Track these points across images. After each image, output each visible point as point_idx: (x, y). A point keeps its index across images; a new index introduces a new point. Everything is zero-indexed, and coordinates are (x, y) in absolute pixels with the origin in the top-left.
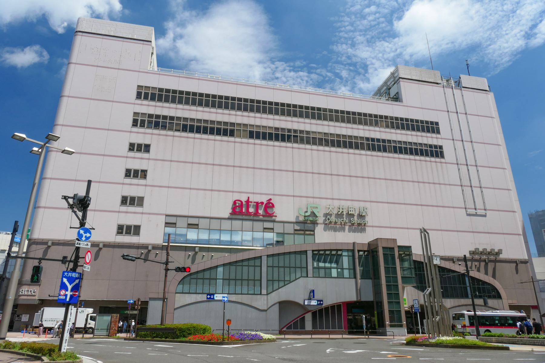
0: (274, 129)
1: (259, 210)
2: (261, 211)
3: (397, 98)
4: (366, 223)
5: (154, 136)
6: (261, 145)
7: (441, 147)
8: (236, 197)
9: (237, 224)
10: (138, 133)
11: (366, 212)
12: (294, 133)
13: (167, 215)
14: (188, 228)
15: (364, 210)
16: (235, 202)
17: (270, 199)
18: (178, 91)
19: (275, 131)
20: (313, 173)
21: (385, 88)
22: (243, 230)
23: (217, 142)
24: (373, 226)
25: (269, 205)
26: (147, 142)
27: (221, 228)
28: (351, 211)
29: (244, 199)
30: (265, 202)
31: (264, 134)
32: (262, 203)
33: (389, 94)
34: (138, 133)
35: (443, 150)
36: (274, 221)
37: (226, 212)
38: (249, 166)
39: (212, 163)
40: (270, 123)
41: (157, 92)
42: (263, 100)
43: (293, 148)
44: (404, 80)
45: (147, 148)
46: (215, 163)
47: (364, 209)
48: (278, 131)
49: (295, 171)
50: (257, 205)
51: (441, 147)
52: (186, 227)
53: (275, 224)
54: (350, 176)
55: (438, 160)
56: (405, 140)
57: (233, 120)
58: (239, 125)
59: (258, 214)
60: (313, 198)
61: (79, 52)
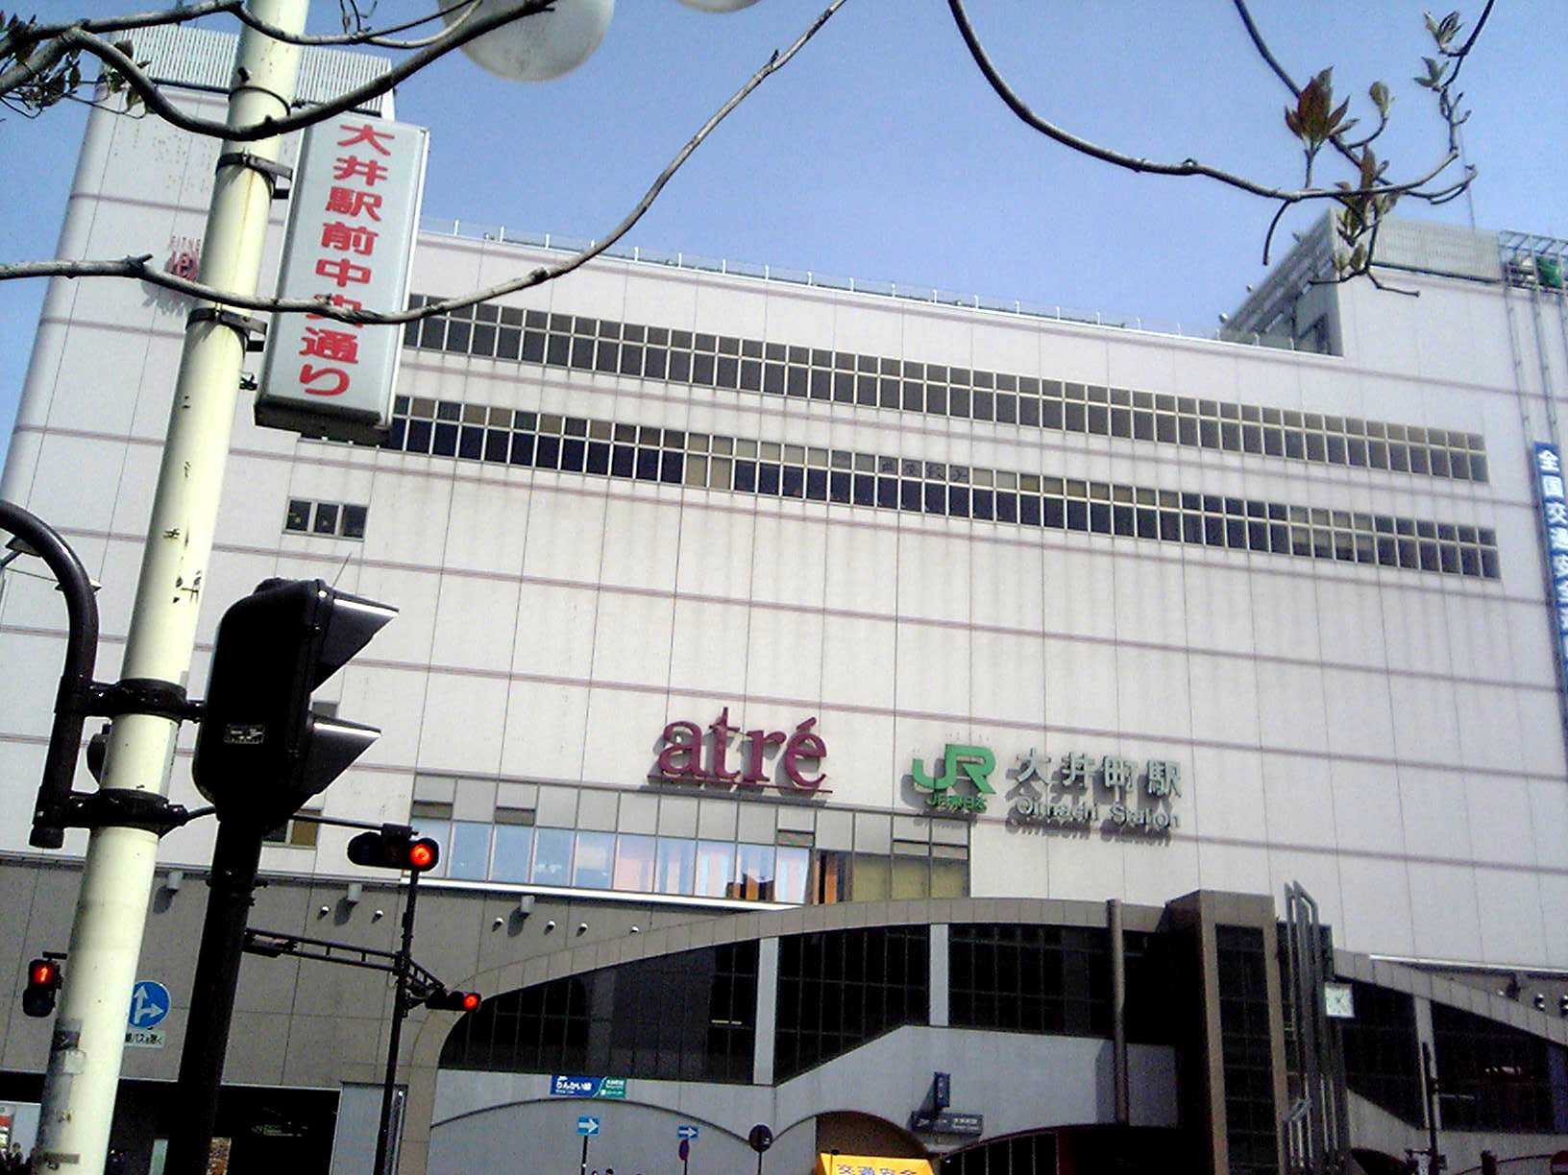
0: (833, 456)
1: (764, 759)
2: (770, 768)
3: (1322, 336)
4: (1173, 821)
5: (382, 476)
6: (658, 502)
7: (1487, 537)
8: (681, 710)
9: (679, 809)
10: (321, 462)
11: (1172, 781)
12: (908, 475)
13: (418, 774)
14: (497, 822)
15: (1164, 776)
16: (668, 735)
17: (812, 721)
18: (622, 327)
19: (833, 465)
20: (971, 627)
21: (1280, 293)
22: (739, 839)
23: (616, 506)
24: (1197, 840)
25: (806, 746)
26: (356, 499)
27: (697, 833)
28: (1115, 777)
29: (704, 716)
30: (790, 732)
31: (793, 478)
32: (777, 738)
33: (1294, 321)
34: (321, 462)
35: (1495, 544)
36: (820, 806)
37: (638, 766)
38: (734, 595)
39: (593, 579)
40: (1170, 479)
41: (498, 324)
42: (654, 325)
43: (971, 538)
44: (204, 97)
45: (354, 521)
46: (605, 582)
47: (1164, 771)
48: (847, 462)
49: (962, 626)
50: (759, 744)
51: (1487, 537)
52: (490, 819)
53: (821, 814)
54: (1116, 643)
55: (1472, 585)
56: (1342, 507)
57: (676, 419)
58: (700, 438)
59: (758, 783)
60: (970, 720)
61: (112, 155)
